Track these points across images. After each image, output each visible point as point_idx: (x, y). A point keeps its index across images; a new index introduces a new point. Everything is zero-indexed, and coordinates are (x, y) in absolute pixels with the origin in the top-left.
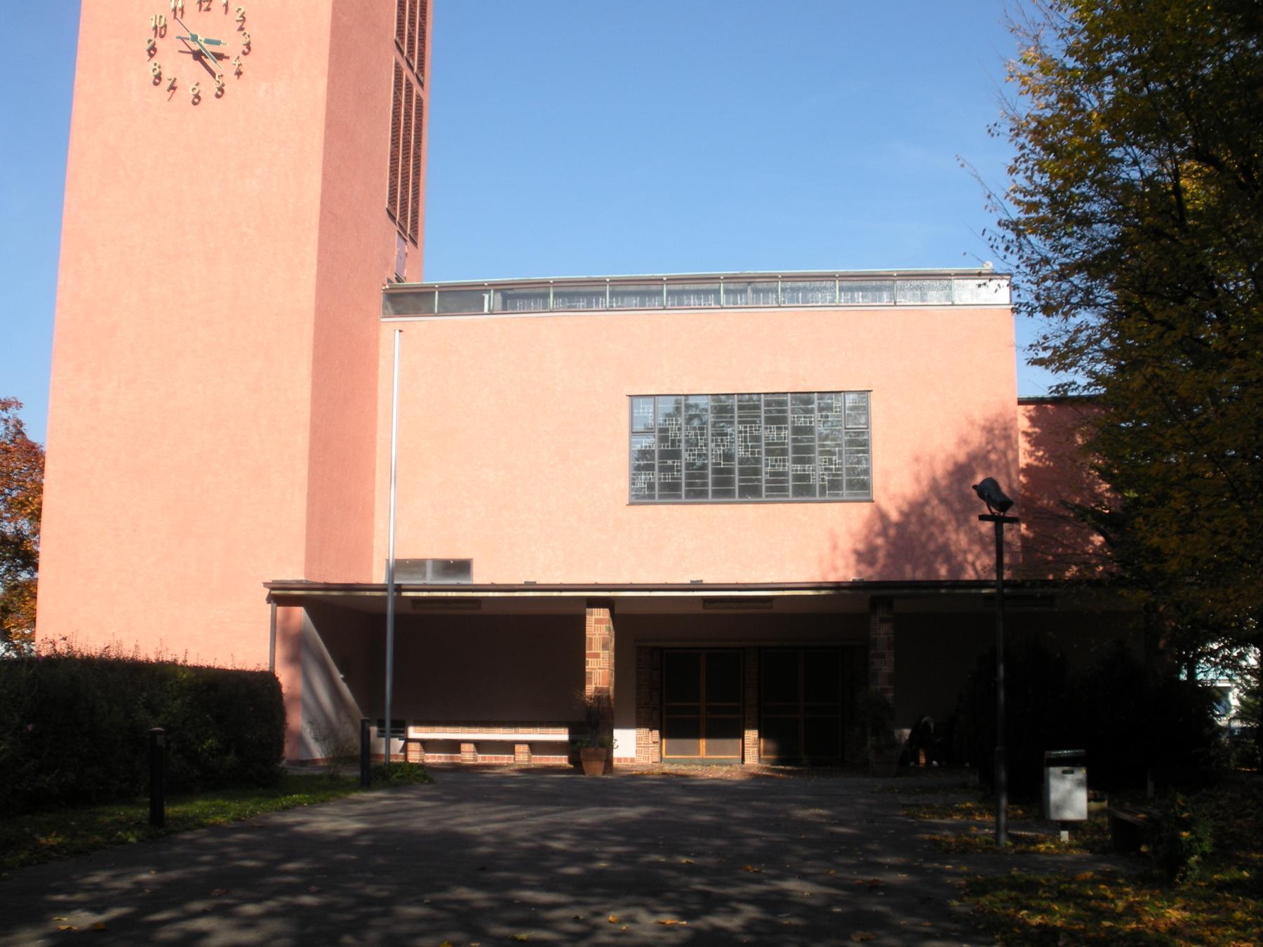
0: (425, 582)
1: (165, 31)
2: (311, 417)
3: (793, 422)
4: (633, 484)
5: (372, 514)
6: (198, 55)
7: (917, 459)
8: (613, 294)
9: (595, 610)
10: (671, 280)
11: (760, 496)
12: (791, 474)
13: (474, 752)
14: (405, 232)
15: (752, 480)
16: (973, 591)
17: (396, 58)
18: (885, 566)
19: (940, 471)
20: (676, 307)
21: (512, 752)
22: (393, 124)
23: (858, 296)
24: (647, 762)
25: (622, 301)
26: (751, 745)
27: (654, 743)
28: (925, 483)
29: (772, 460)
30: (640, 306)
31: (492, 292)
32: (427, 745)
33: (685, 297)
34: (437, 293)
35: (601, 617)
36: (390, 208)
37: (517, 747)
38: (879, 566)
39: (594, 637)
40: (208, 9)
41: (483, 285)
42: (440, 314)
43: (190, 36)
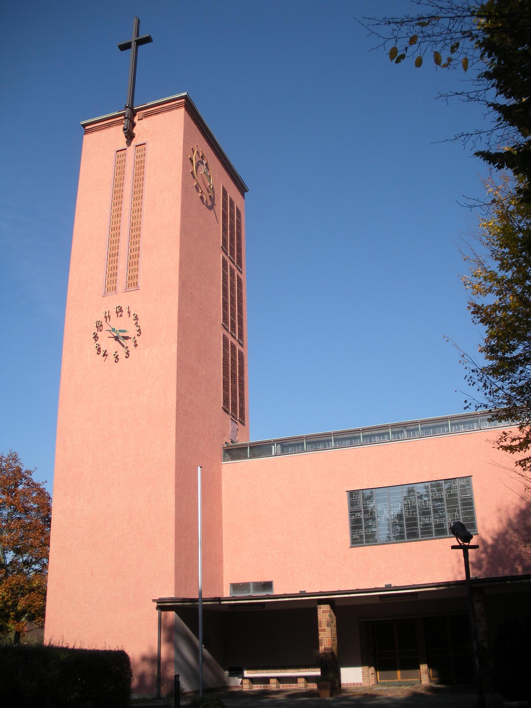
0: (249, 594)
1: (102, 328)
2: (176, 514)
3: (432, 497)
4: (352, 537)
5: (222, 561)
6: (117, 338)
7: (499, 510)
8: (335, 440)
9: (322, 606)
10: (364, 430)
11: (418, 537)
12: (433, 524)
13: (277, 683)
14: (236, 419)
15: (413, 529)
16: (525, 581)
17: (223, 333)
18: (487, 569)
19: (512, 514)
20: (368, 444)
21: (296, 682)
22: (223, 365)
23: (461, 427)
24: (369, 685)
25: (341, 443)
26: (424, 673)
27: (372, 674)
28: (505, 522)
29: (423, 518)
30: (350, 445)
31: (275, 444)
32: (253, 680)
33: (373, 438)
34: (248, 447)
35: (326, 609)
36: (224, 407)
37: (298, 679)
38: (484, 569)
39: (322, 620)
40: (121, 316)
41: (271, 441)
42: (250, 458)
43: (111, 329)
